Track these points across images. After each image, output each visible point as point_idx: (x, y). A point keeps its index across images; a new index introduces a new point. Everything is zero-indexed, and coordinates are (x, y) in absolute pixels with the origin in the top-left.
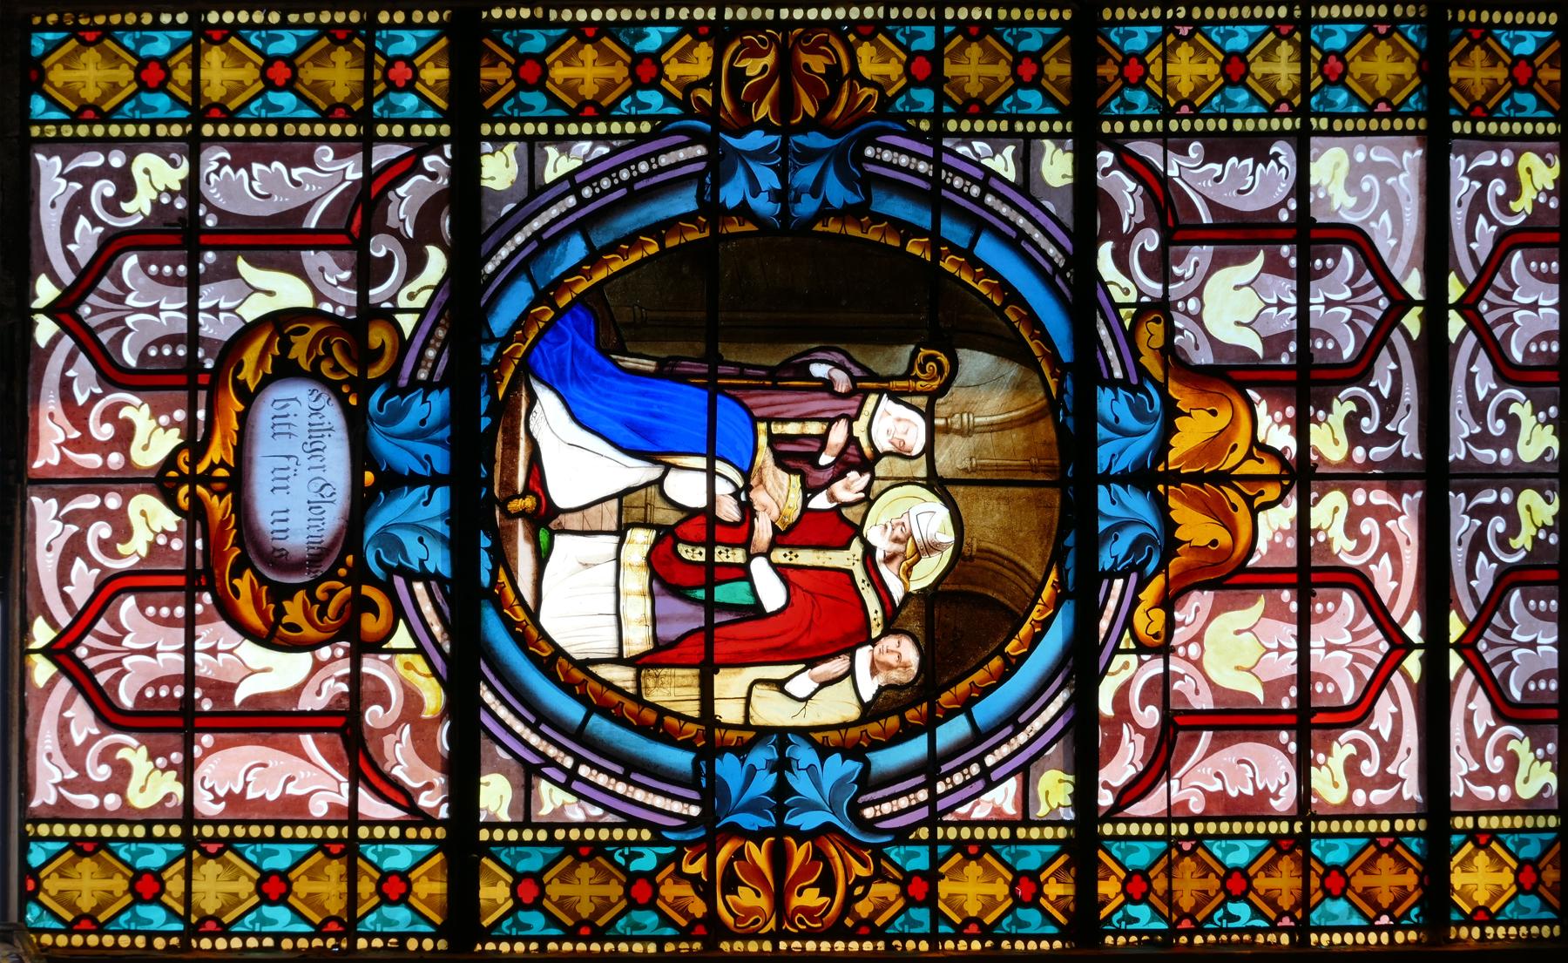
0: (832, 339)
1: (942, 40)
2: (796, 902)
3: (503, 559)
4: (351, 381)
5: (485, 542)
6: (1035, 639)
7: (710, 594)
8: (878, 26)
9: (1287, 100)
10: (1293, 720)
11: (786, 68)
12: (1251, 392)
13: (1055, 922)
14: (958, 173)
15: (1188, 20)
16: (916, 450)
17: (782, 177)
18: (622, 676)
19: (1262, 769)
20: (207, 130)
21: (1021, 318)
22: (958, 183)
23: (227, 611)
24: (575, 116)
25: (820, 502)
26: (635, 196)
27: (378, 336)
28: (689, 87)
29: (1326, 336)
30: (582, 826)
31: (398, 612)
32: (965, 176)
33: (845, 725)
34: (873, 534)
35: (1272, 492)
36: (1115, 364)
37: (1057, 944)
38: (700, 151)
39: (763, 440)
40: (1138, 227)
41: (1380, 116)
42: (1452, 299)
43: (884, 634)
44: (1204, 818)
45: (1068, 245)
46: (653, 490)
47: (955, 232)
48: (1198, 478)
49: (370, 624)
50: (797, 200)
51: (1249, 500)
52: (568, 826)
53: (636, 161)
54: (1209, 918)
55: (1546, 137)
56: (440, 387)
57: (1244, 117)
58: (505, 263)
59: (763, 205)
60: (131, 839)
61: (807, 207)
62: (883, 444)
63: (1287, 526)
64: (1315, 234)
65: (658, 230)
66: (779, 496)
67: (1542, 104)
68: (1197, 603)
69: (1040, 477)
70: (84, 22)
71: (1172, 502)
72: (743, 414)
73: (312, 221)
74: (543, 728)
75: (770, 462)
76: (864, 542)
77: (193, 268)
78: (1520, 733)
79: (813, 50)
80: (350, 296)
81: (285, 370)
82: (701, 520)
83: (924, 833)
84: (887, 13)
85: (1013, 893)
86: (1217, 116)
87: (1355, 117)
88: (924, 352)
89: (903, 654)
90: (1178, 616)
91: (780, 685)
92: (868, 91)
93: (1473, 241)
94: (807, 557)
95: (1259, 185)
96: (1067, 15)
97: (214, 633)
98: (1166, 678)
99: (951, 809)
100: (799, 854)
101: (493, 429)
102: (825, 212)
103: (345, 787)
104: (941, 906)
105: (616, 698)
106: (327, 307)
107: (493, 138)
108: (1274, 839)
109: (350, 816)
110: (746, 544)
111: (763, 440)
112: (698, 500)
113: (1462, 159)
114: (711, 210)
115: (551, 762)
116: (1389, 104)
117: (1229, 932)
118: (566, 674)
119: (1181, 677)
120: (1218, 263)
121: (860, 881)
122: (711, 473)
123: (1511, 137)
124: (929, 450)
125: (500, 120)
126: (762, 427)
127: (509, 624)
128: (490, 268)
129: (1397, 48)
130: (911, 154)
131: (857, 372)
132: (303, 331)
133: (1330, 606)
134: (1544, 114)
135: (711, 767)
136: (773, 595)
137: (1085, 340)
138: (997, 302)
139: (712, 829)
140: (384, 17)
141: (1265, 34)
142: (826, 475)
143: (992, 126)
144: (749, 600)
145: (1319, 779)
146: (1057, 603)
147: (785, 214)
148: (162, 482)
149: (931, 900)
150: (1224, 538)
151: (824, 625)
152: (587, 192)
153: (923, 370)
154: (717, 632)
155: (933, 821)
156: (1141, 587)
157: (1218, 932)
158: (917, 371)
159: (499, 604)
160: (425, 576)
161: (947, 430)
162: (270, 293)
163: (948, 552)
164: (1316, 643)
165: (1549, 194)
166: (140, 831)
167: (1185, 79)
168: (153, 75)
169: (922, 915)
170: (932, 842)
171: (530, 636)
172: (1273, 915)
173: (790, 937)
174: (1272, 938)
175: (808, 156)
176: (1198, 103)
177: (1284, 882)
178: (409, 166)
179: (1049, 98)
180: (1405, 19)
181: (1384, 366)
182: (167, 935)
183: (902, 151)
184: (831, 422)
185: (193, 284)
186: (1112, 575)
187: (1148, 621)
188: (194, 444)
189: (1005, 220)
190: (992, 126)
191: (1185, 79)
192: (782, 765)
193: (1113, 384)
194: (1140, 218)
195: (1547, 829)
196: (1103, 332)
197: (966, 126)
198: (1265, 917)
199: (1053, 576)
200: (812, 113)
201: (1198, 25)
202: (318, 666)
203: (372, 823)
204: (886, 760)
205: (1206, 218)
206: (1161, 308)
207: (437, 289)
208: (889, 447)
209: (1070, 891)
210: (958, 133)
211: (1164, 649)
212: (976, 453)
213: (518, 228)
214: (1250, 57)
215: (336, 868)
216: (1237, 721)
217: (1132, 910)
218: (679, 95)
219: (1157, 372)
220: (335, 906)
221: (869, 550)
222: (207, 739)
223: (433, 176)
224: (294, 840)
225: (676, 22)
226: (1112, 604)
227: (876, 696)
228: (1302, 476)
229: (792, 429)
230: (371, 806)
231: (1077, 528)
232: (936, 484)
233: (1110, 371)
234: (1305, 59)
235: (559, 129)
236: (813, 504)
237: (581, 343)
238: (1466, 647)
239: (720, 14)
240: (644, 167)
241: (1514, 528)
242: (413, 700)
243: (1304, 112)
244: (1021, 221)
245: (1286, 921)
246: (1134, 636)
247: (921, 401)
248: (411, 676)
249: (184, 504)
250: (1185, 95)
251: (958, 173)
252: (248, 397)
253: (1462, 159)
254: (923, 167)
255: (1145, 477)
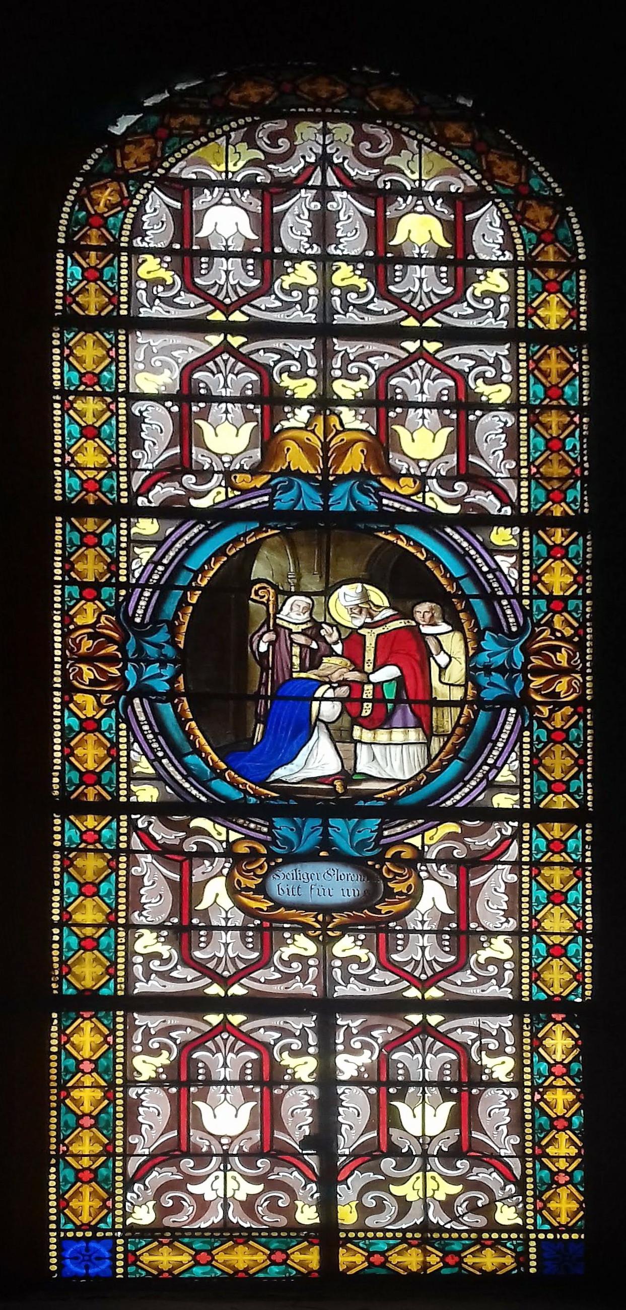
0: (243, 640)
1: (73, 582)
2: (565, 664)
3: (370, 795)
4: (268, 861)
5: (361, 803)
6: (418, 545)
7: (390, 701)
8: (64, 613)
9: (108, 405)
10: (463, 413)
11: (88, 659)
12: (276, 430)
13: (577, 538)
14: (150, 576)
15: (62, 456)
16: (309, 601)
17: (154, 662)
18: (436, 745)
19: (490, 430)
20: (121, 921)
21: (233, 547)
22: (156, 577)
23: (400, 916)
24: (116, 759)
25: (338, 648)
26: (163, 731)
27: (242, 849)
28: (100, 706)
29: (244, 388)
30: (522, 763)
31: (401, 842)
32: (152, 573)
33: (465, 639)
34: (358, 623)
35: (334, 420)
36: (260, 500)
37: (589, 537)
38: (137, 701)
39: (303, 675)
40: (182, 485)
41: (117, 354)
42: (223, 318)
43: (414, 619)
44: (518, 461)
45: (192, 522)
46: (330, 726)
47: (184, 579)
48: (326, 459)
49: (407, 854)
50: (165, 656)
51: (338, 432)
52: (521, 769)
53: (142, 731)
54: (575, 460)
55: (129, 262)
56: (271, 822)
57: (118, 428)
58: (200, 792)
59: (168, 672)
60: (530, 958)
61: (169, 651)
62: (305, 617)
63: (353, 412)
64: (185, 392)
65: (182, 722)
66: (334, 666)
67: (110, 264)
68: (395, 460)
69: (325, 540)
70: (57, 973)
71: (339, 472)
72: (287, 684)
73: (176, 877)
74: (466, 778)
75: (315, 671)
76: (360, 628)
77: (202, 928)
78: (471, 289)
79: (79, 646)
80: (219, 862)
81: (261, 890)
82: (348, 704)
83: (526, 602)
84: (57, 610)
85: (561, 559)
86: (118, 443)
87: (118, 368)
88: (253, 596)
89: (423, 609)
90: (404, 472)
91: (442, 670)
92: (103, 619)
93: (190, 306)
94: (370, 655)
95: (158, 423)
96: (59, 519)
97: (412, 921)
98: (438, 477)
99: (513, 589)
100: (536, 661)
101: (296, 799)
102: (173, 643)
103: (500, 867)
104: (568, 593)
105: (449, 745)
106: (225, 871)
107: (128, 796)
108: (530, 424)
109: (517, 865)
110: (362, 684)
111: (303, 675)
112: (338, 706)
113: (142, 310)
114: (171, 696)
115: (486, 776)
116: (111, 349)
117: (582, 449)
118: (435, 768)
119: (438, 471)
120: (203, 445)
121: (553, 633)
122: (322, 699)
123: (129, 282)
124: (307, 595)
125: (118, 793)
126: (295, 675)
127: (408, 793)
128: (203, 799)
129: (78, 343)
130: (139, 599)
131: (265, 629)
132: (239, 882)
133: (398, 391)
134: (115, 262)
135: (488, 702)
136: (390, 672)
137: (247, 515)
138: (225, 559)
139: (524, 704)
140: (57, 844)
141: (69, 415)
142: (323, 645)
143: (123, 559)
144: (394, 684)
145: (497, 399)
146: (396, 533)
147: (174, 662)
148: (326, 943)
149: (565, 599)
150: (359, 446)
151: (412, 650)
152: (160, 754)
153: (263, 597)
154: (412, 697)
155: (519, 597)
156: (388, 491)
157: (582, 456)
158: (264, 600)
159: (396, 797)
160: (380, 830)
161: (297, 585)
162: (217, 895)
163: (367, 587)
164: (420, 398)
165: (162, 261)
166: (526, 954)
167: (96, 459)
168: (88, 944)
169: (572, 604)
170: (531, 598)
171: (415, 784)
172: (573, 427)
173: (585, 668)
174: (585, 427)
175: (140, 649)
176: (110, 453)
177: (554, 419)
178: (144, 835)
179: (108, 529)
180: (61, 339)
181: (261, 357)
182: (584, 943)
183: (137, 604)
184: (292, 642)
185: (210, 928)
186: (380, 504)
187: (407, 486)
188: (304, 929)
189: (177, 554)
190: (123, 559)
191: (96, 459)
192: (488, 669)
193: (271, 501)
194: (177, 484)
195: (526, 275)
196: (242, 505)
197: (123, 572)
198: (574, 430)
199: (382, 535)
200: (116, 647)
201: (65, 451)
202: (431, 877)
203: (521, 855)
204: (484, 618)
205: (177, 450)
206: (227, 474)
207: (215, 822)
208: (307, 615)
209: (559, 531)
210: (127, 576)
211: (423, 479)
212: (311, 571)
213: (181, 785)
214: (83, 424)
215: (546, 871)
216: (463, 442)
217: (570, 499)
218: (104, 710)
219: (266, 478)
220: (568, 872)
221: (365, 625)
222: (473, 925)
223: (150, 823)
224: (530, 889)
225: (62, 711)
226: (397, 505)
227: (448, 624)
228: (325, 402)
229: (296, 661)
230: (512, 854)
231: (356, 523)
232: (327, 592)
233: (264, 502)
234: (85, 394)
235: (123, 766)
236: (339, 652)
237: (247, 758)
238: (421, 317)
239: (57, 689)
240: (146, 728)
241: (354, 288)
242: (450, 836)
243: (115, 396)
244: (178, 545)
245: (576, 419)
246: (416, 494)
247: (281, 599)
248: (213, 494)
249: (338, 933)
250: (106, 459)
251: (150, 576)
252: (278, 905)
253: (142, 310)
254: (147, 594)
255: (325, 488)
